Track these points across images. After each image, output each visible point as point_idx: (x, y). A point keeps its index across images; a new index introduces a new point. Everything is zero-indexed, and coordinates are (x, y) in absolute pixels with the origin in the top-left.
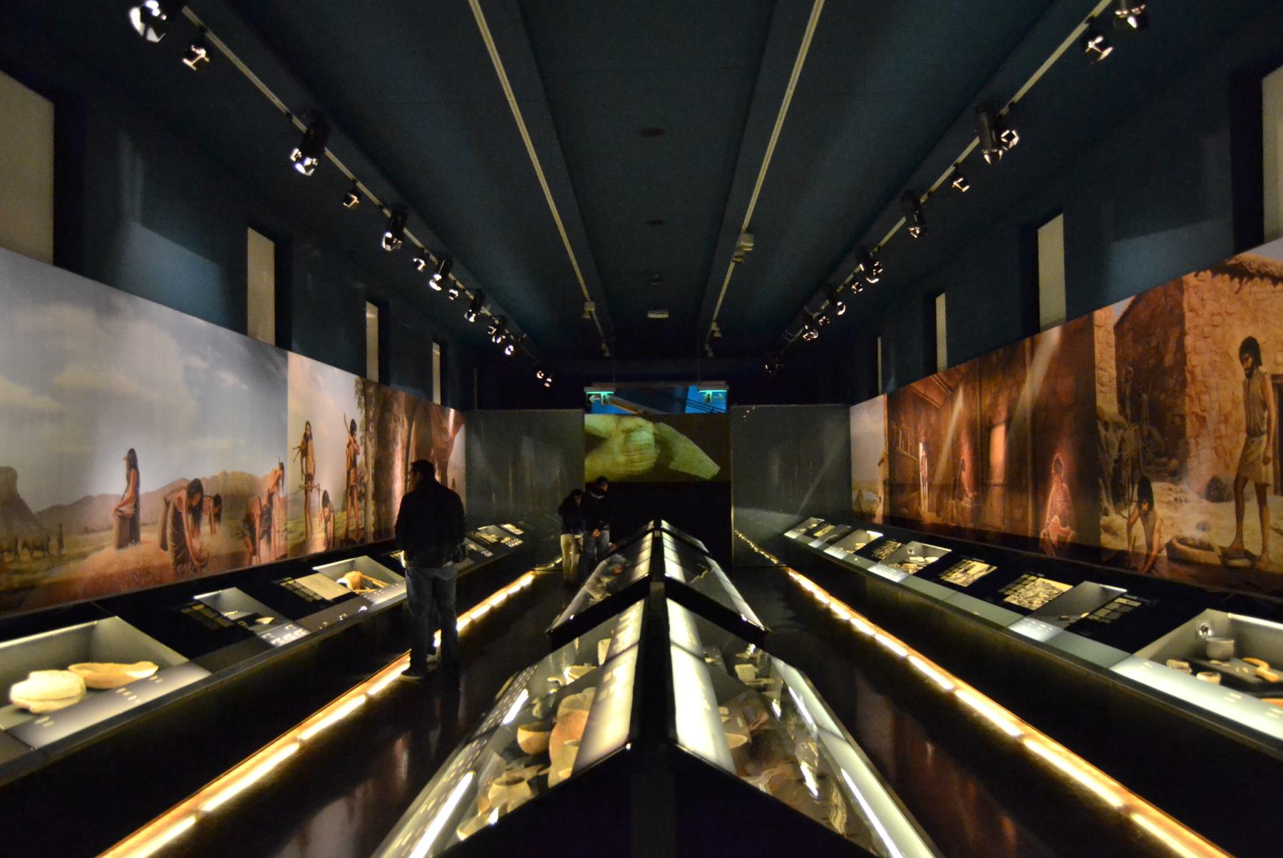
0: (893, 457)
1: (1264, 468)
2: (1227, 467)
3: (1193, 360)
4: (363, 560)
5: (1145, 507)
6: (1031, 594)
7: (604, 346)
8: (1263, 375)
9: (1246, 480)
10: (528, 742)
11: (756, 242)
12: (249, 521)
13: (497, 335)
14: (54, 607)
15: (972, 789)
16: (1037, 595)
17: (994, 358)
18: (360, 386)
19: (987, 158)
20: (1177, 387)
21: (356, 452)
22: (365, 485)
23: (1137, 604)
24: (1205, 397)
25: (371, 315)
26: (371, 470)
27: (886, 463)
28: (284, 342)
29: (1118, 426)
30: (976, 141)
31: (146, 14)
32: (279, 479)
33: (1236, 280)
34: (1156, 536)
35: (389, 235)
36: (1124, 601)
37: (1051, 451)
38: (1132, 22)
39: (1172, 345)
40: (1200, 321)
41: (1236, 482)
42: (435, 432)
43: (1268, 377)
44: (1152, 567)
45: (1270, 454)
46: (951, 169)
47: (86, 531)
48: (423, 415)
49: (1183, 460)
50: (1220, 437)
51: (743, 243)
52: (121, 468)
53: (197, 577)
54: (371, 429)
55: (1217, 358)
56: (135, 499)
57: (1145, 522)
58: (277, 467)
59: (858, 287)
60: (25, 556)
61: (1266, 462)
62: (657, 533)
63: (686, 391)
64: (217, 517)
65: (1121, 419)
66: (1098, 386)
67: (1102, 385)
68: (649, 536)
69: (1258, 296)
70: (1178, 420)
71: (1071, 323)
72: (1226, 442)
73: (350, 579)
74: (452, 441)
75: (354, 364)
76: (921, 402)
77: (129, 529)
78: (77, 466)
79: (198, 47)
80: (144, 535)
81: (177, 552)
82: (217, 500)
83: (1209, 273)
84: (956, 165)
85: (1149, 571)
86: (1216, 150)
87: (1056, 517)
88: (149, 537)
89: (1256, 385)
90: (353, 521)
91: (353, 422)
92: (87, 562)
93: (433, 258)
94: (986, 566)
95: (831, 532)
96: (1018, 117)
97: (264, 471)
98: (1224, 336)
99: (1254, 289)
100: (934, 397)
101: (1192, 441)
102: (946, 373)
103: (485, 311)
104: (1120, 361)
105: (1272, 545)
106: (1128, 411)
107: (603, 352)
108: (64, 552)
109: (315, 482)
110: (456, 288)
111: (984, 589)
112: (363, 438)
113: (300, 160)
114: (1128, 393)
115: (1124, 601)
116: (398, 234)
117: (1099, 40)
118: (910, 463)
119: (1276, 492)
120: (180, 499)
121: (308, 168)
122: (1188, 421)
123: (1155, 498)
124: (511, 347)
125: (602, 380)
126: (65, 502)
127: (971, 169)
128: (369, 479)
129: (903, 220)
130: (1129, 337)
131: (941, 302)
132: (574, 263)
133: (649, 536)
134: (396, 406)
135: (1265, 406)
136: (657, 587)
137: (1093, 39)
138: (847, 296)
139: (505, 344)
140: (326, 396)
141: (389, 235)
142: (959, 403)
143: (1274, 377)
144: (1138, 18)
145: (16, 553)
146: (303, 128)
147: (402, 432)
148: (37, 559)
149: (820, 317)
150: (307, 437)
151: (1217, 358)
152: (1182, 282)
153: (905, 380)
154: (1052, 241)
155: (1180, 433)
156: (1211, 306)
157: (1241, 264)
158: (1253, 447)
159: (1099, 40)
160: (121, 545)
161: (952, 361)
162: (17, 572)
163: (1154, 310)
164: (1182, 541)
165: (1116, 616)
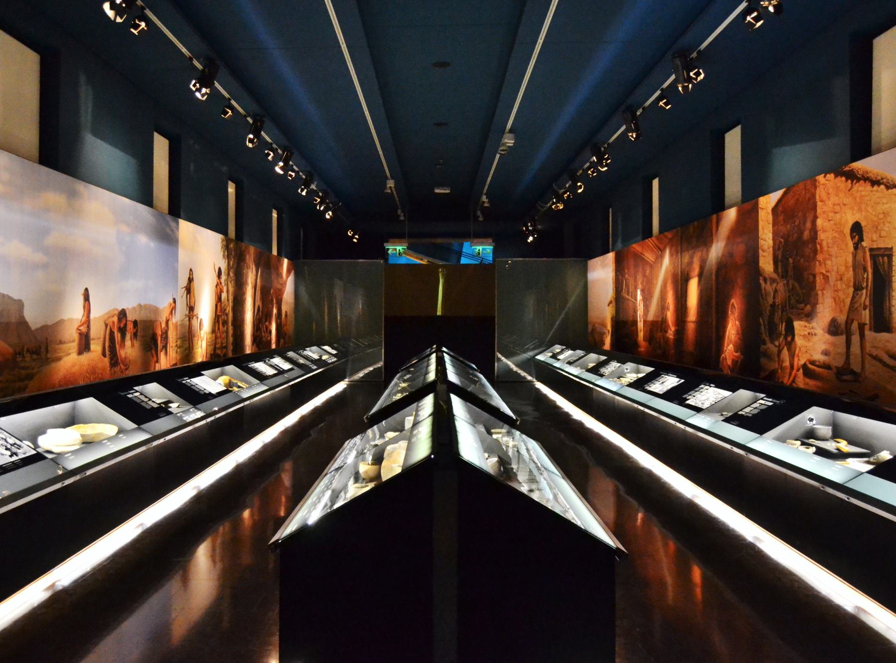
0: (619, 300)
1: (863, 312)
2: (841, 311)
3: (822, 236)
4: (231, 368)
5: (789, 339)
6: (704, 398)
7: (399, 212)
8: (864, 248)
9: (852, 321)
10: (366, 472)
11: (516, 139)
12: (154, 338)
13: (321, 204)
14: (44, 392)
15: (672, 544)
16: (708, 399)
17: (691, 230)
18: (225, 243)
19: (680, 89)
20: (812, 255)
21: (221, 291)
22: (227, 315)
23: (771, 404)
24: (829, 262)
25: (231, 189)
26: (231, 304)
27: (614, 304)
28: (175, 210)
29: (773, 281)
30: (673, 77)
31: (113, 6)
32: (173, 309)
33: (849, 181)
34: (796, 359)
35: (251, 136)
36: (763, 402)
37: (728, 298)
38: (771, 9)
39: (809, 225)
40: (825, 209)
41: (847, 322)
42: (274, 276)
43: (867, 249)
44: (793, 381)
45: (867, 303)
46: (658, 92)
47: (61, 342)
48: (267, 266)
49: (814, 305)
50: (836, 291)
51: (506, 141)
52: (81, 300)
53: (124, 376)
54: (231, 274)
55: (836, 235)
56: (88, 322)
57: (789, 350)
58: (171, 301)
59: (593, 172)
60: (28, 357)
61: (865, 309)
62: (440, 354)
63: (462, 245)
64: (135, 335)
65: (775, 276)
66: (760, 251)
67: (763, 251)
68: (434, 355)
69: (863, 193)
70: (811, 277)
71: (746, 204)
72: (840, 294)
73: (224, 380)
74: (285, 283)
75: (219, 226)
76: (638, 257)
77: (84, 344)
78: (55, 299)
79: (140, 21)
80: (93, 347)
81: (111, 359)
82: (135, 323)
83: (832, 175)
84: (662, 90)
85: (791, 384)
86: (841, 88)
87: (731, 346)
88: (96, 347)
89: (860, 254)
90: (219, 341)
91: (220, 269)
92: (62, 363)
93: (280, 151)
94: (678, 379)
95: (571, 356)
96: (704, 59)
97: (164, 304)
98: (841, 220)
99: (860, 189)
100: (649, 256)
101: (820, 293)
102: (657, 238)
103: (313, 187)
104: (775, 234)
105: (867, 366)
106: (780, 271)
107: (399, 216)
108: (49, 356)
109: (195, 312)
110: (293, 171)
111: (676, 396)
112: (227, 280)
113: (199, 90)
114: (780, 257)
115: (763, 402)
116: (257, 135)
117: (755, 14)
118: (631, 304)
119: (870, 329)
120: (113, 322)
121: (203, 95)
122: (818, 279)
123: (796, 332)
124: (330, 213)
125: (398, 237)
126: (49, 323)
127: (669, 94)
128: (229, 310)
129: (624, 127)
130: (781, 218)
131: (656, 183)
132: (381, 153)
133: (434, 355)
134: (248, 257)
135: (865, 270)
136: (441, 387)
137: (750, 15)
138: (585, 178)
139: (326, 210)
140: (203, 249)
141: (251, 136)
142: (666, 261)
143: (871, 250)
144: (774, 6)
145: (24, 356)
146: (199, 66)
147: (251, 277)
148: (35, 360)
149: (565, 193)
150: (190, 280)
151: (836, 235)
152: (816, 180)
153: (628, 239)
154: (733, 140)
155: (812, 287)
156: (834, 199)
157: (852, 171)
158: (857, 297)
159: (755, 14)
160: (80, 353)
161: (662, 230)
162: (23, 368)
163: (798, 200)
164: (813, 363)
165: (756, 411)
